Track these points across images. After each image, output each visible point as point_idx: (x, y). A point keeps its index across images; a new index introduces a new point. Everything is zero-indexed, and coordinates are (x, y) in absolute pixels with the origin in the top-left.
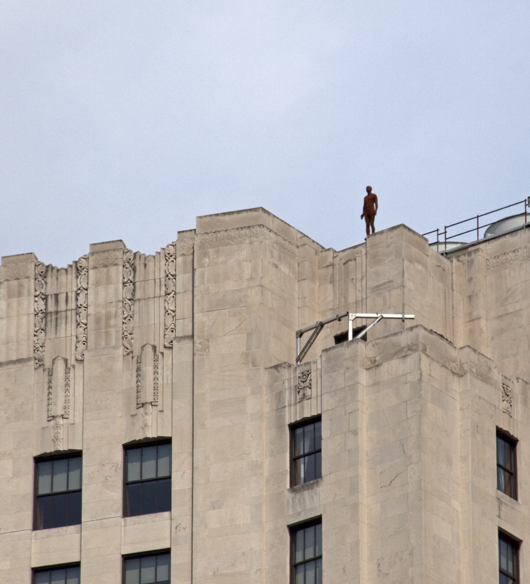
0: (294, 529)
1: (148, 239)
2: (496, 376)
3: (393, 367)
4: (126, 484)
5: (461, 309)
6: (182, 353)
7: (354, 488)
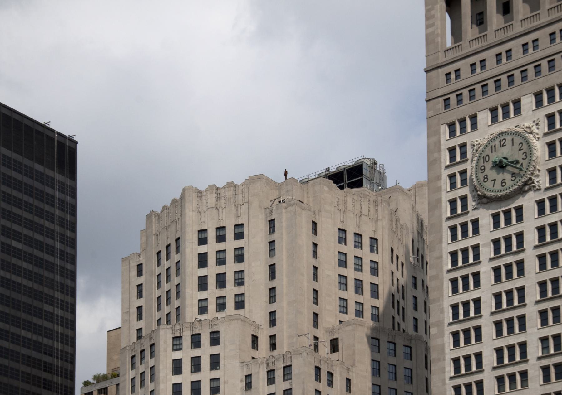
0: (270, 313)
1: (239, 181)
2: (312, 210)
3: (290, 208)
4: (235, 233)
5: (306, 195)
6: (246, 205)
7: (282, 234)
